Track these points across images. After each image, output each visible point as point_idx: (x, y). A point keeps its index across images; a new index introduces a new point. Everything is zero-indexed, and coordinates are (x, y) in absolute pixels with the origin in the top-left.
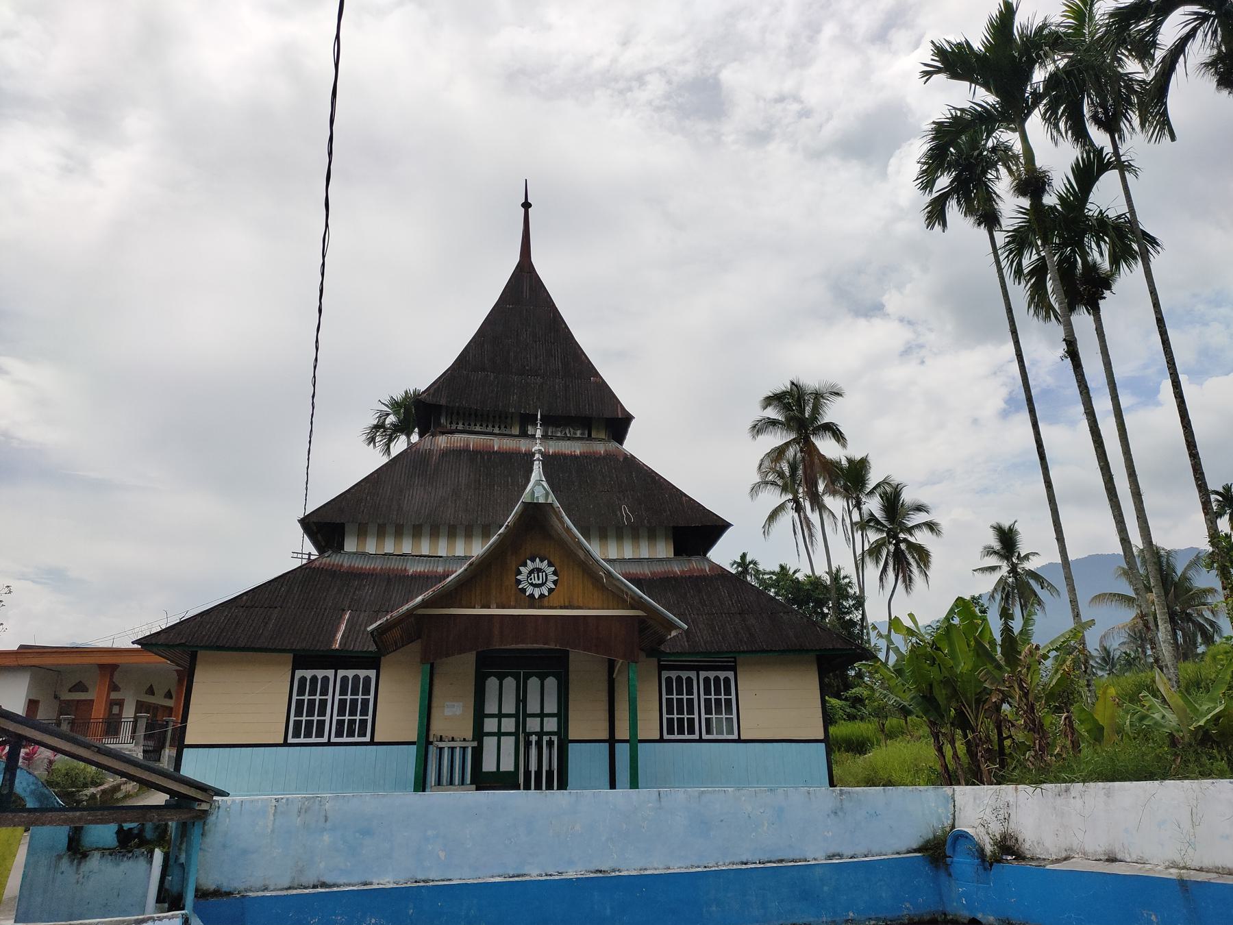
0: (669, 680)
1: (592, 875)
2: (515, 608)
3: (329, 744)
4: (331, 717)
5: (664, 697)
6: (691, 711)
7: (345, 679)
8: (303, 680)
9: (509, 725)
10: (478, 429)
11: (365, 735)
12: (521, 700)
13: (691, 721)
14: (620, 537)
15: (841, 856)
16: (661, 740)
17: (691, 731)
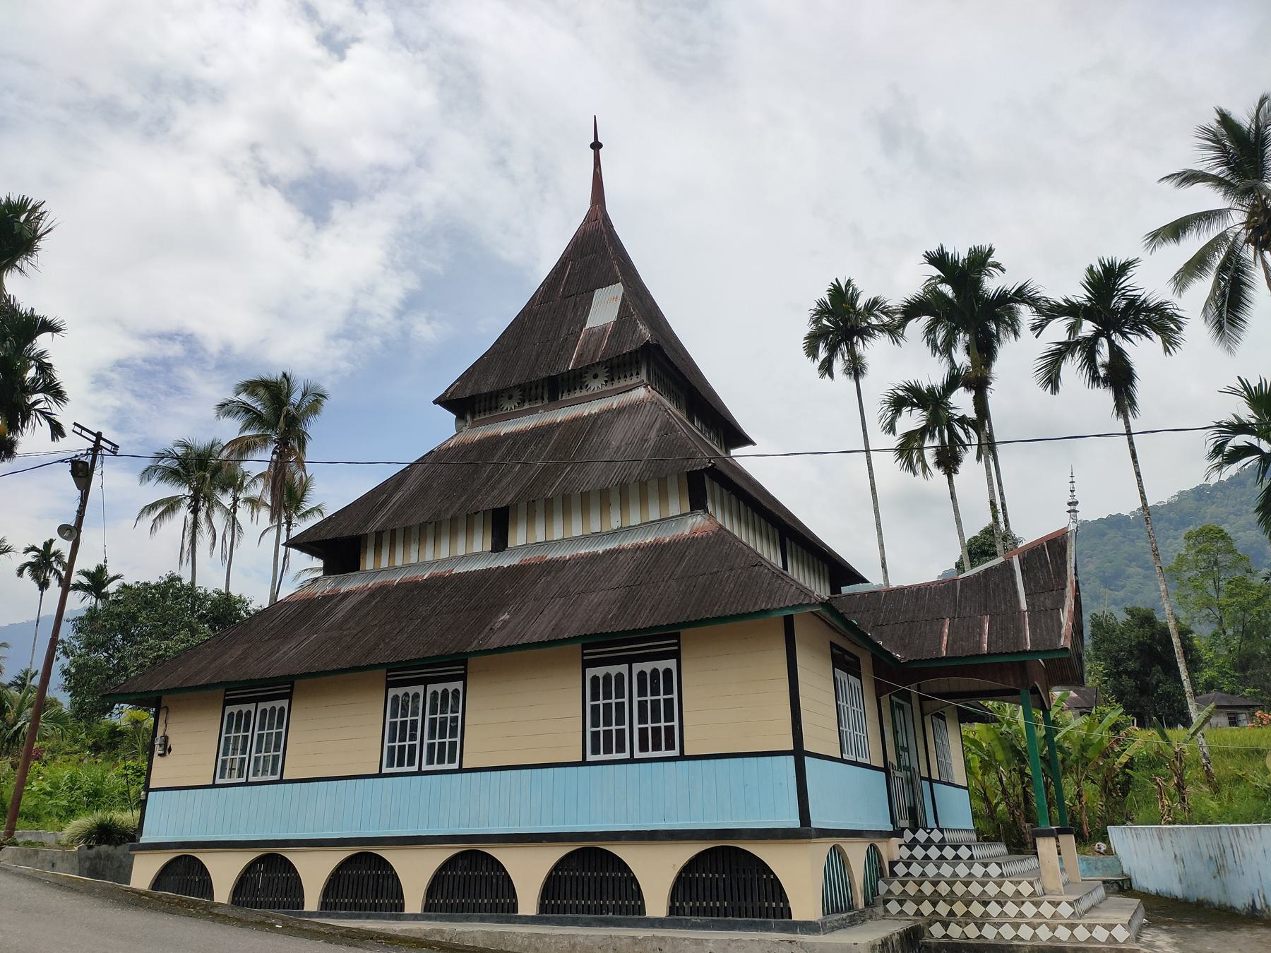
3: (632, 760)
4: (633, 726)
5: (589, 703)
7: (642, 675)
8: (595, 679)
16: (584, 763)
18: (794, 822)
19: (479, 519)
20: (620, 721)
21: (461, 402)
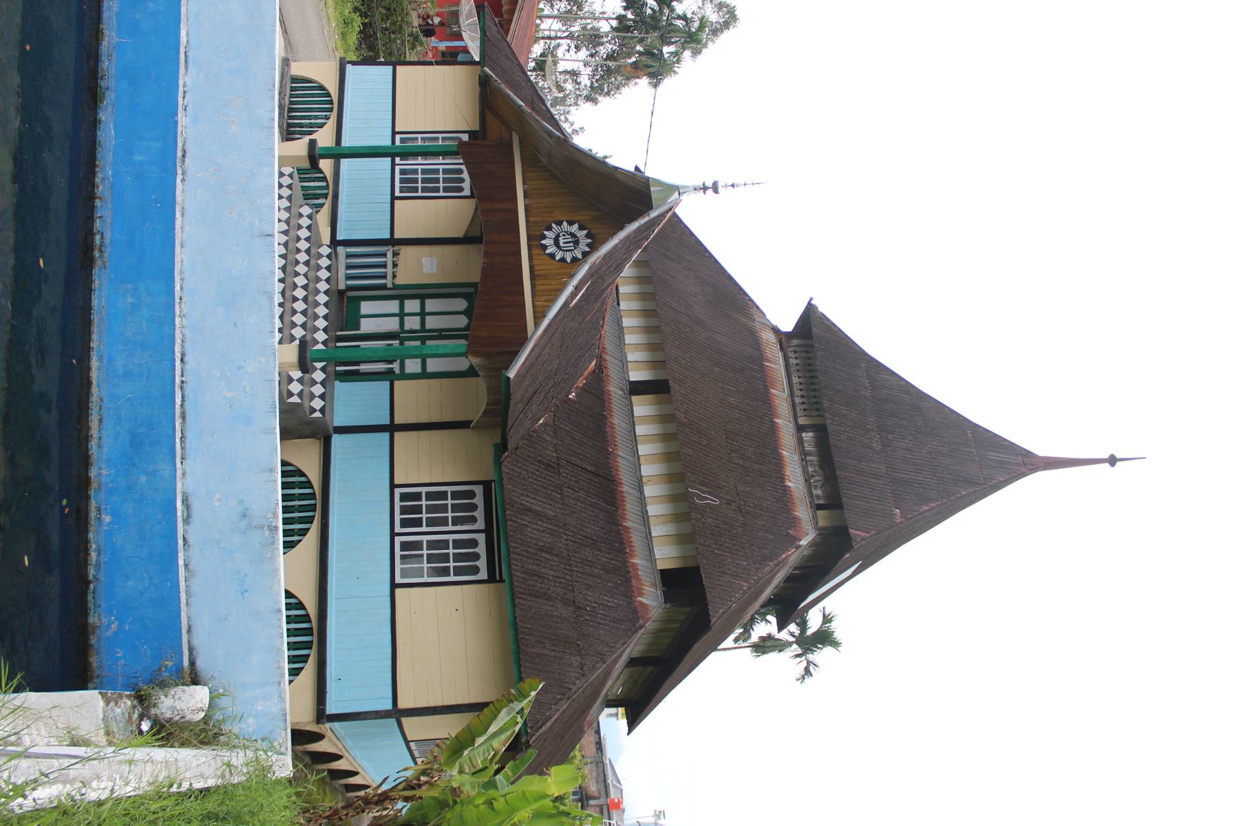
0: (471, 495)
1: (180, 145)
2: (527, 222)
5: (449, 489)
6: (431, 522)
9: (412, 323)
10: (795, 380)
13: (418, 523)
14: (674, 498)
15: (187, 521)
16: (393, 486)
17: (404, 523)
18: (331, 709)
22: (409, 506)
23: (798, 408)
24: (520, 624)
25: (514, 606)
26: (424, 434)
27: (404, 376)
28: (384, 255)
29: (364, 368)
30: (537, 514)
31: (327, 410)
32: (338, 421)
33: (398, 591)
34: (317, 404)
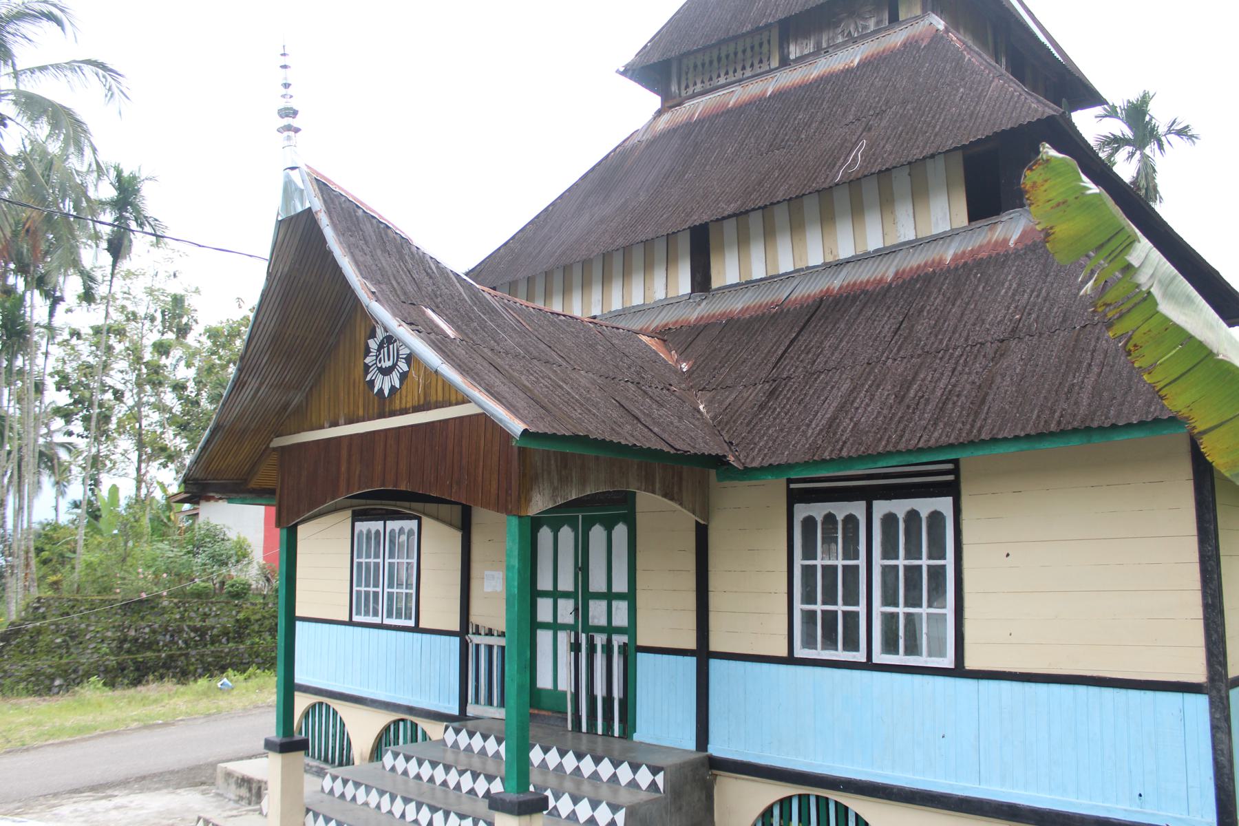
0: (809, 523)
5: (799, 562)
9: (566, 611)
11: (942, 654)
12: (582, 569)
16: (790, 660)
17: (851, 644)
19: (936, 170)
20: (851, 598)
21: (659, 69)
22: (828, 633)
23: (759, 71)
24: (1030, 430)
25: (994, 441)
26: (714, 601)
27: (631, 630)
28: (477, 646)
29: (617, 693)
30: (841, 408)
31: (658, 761)
32: (688, 742)
33: (970, 664)
34: (644, 777)
